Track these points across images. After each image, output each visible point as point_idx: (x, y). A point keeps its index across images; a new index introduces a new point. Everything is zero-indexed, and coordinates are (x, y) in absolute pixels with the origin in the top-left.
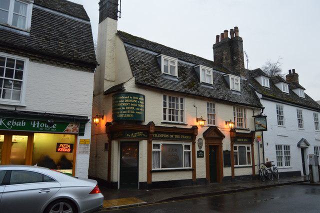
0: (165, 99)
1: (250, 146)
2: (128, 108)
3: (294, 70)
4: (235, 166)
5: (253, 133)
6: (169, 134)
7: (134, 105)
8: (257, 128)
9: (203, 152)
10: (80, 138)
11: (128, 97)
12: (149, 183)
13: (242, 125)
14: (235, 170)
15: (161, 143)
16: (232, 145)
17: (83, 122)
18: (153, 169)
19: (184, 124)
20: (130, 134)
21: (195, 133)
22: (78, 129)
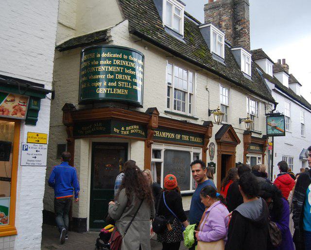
1: (261, 156)
2: (120, 77)
3: (284, 60)
5: (265, 138)
8: (270, 132)
9: (214, 165)
10: (27, 129)
15: (162, 147)
17: (38, 96)
22: (24, 108)
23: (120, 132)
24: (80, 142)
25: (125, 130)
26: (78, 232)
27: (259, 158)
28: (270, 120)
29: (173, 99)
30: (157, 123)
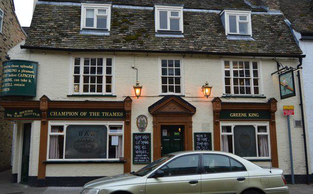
0: (77, 62)
5: (273, 101)
6: (79, 110)
7: (12, 75)
12: (41, 178)
16: (216, 124)
18: (48, 160)
19: (111, 96)
20: (13, 114)
21: (272, 109)
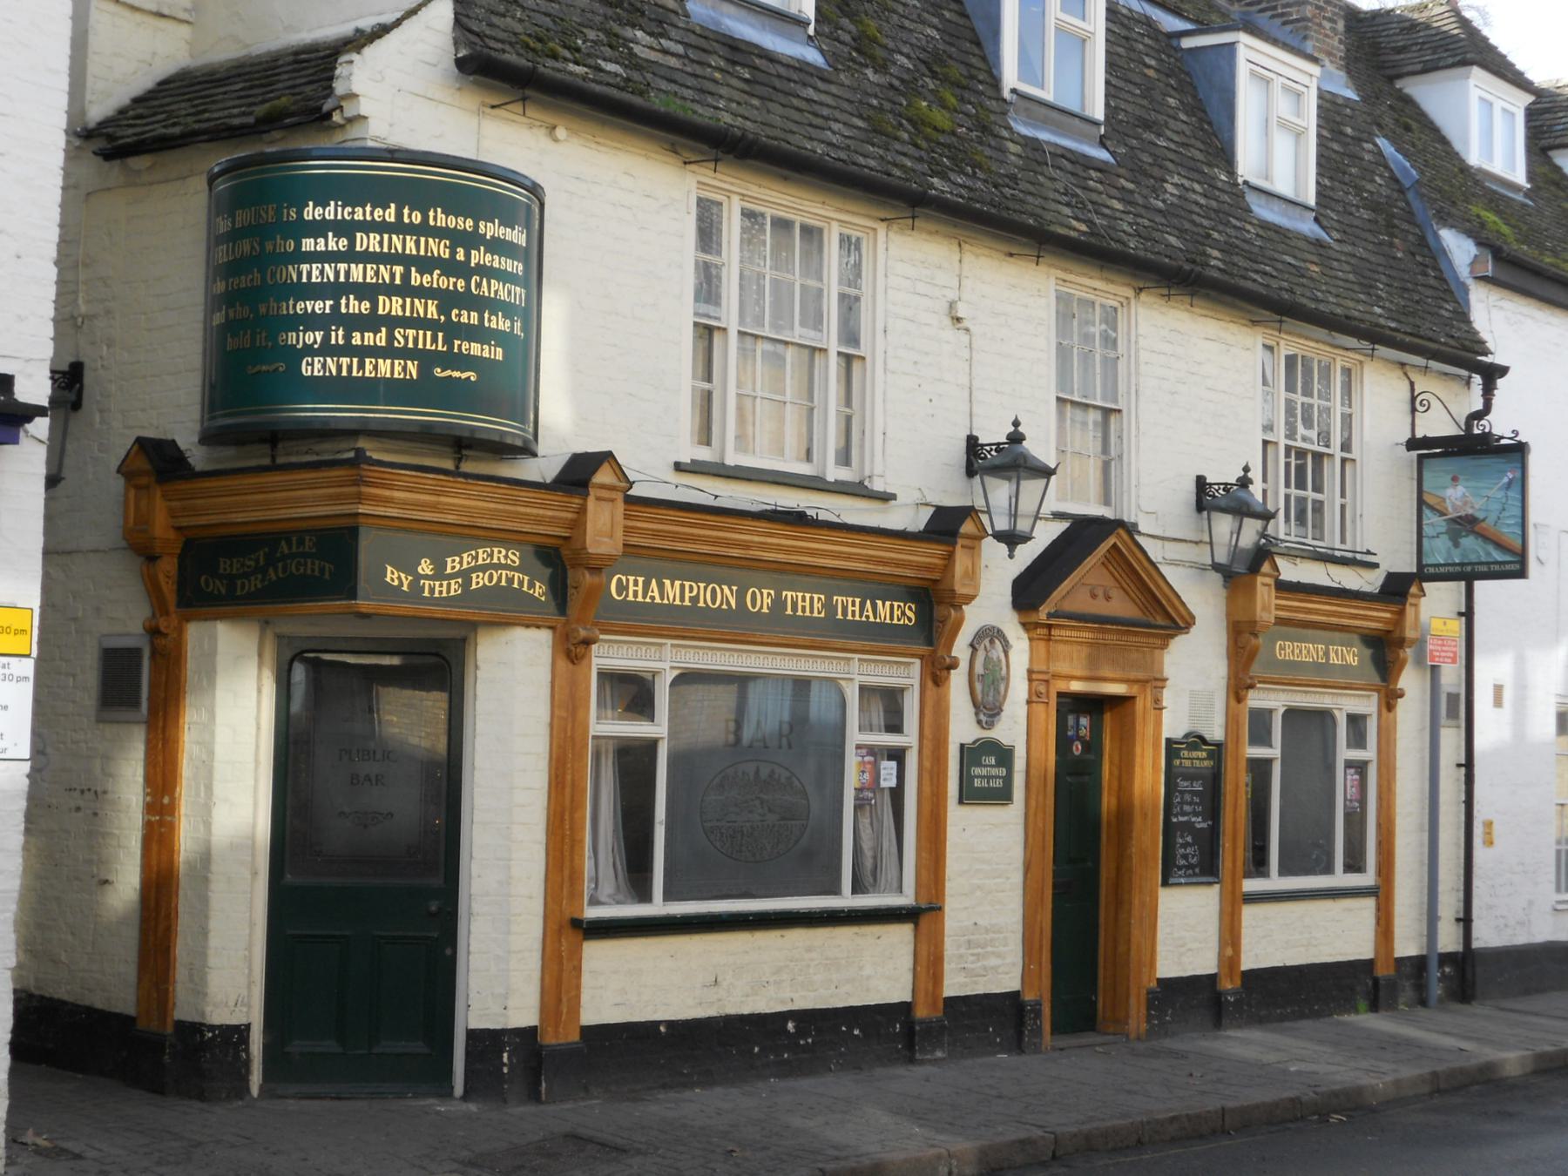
4: (1251, 885)
7: (436, 280)
8: (1440, 551)
9: (1004, 755)
11: (390, 215)
13: (1319, 526)
14: (1249, 913)
18: (592, 913)
20: (410, 568)
23: (416, 586)
24: (213, 639)
25: (439, 574)
26: (201, 1097)
27: (1356, 721)
28: (1437, 476)
29: (1338, 501)
30: (619, 533)
